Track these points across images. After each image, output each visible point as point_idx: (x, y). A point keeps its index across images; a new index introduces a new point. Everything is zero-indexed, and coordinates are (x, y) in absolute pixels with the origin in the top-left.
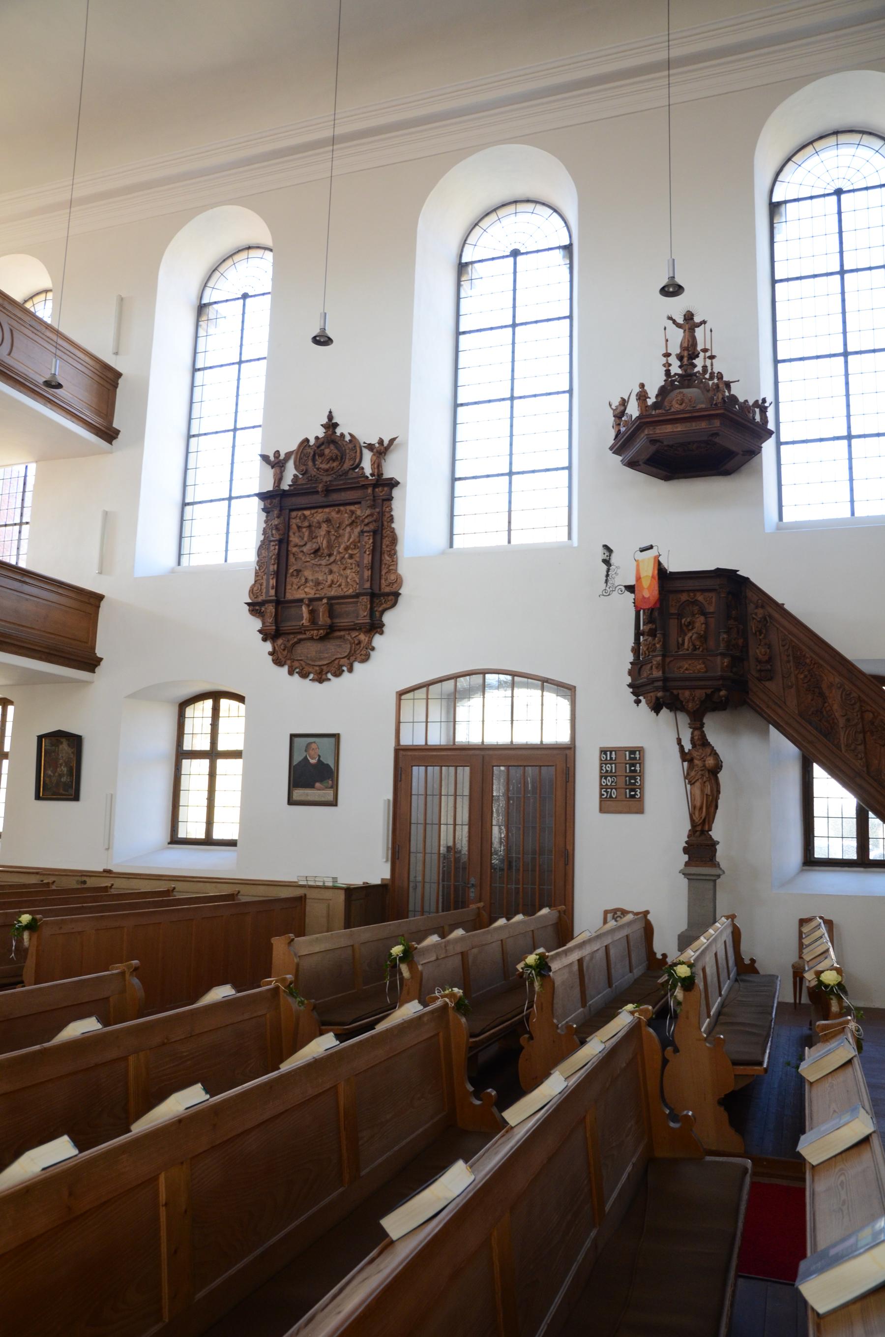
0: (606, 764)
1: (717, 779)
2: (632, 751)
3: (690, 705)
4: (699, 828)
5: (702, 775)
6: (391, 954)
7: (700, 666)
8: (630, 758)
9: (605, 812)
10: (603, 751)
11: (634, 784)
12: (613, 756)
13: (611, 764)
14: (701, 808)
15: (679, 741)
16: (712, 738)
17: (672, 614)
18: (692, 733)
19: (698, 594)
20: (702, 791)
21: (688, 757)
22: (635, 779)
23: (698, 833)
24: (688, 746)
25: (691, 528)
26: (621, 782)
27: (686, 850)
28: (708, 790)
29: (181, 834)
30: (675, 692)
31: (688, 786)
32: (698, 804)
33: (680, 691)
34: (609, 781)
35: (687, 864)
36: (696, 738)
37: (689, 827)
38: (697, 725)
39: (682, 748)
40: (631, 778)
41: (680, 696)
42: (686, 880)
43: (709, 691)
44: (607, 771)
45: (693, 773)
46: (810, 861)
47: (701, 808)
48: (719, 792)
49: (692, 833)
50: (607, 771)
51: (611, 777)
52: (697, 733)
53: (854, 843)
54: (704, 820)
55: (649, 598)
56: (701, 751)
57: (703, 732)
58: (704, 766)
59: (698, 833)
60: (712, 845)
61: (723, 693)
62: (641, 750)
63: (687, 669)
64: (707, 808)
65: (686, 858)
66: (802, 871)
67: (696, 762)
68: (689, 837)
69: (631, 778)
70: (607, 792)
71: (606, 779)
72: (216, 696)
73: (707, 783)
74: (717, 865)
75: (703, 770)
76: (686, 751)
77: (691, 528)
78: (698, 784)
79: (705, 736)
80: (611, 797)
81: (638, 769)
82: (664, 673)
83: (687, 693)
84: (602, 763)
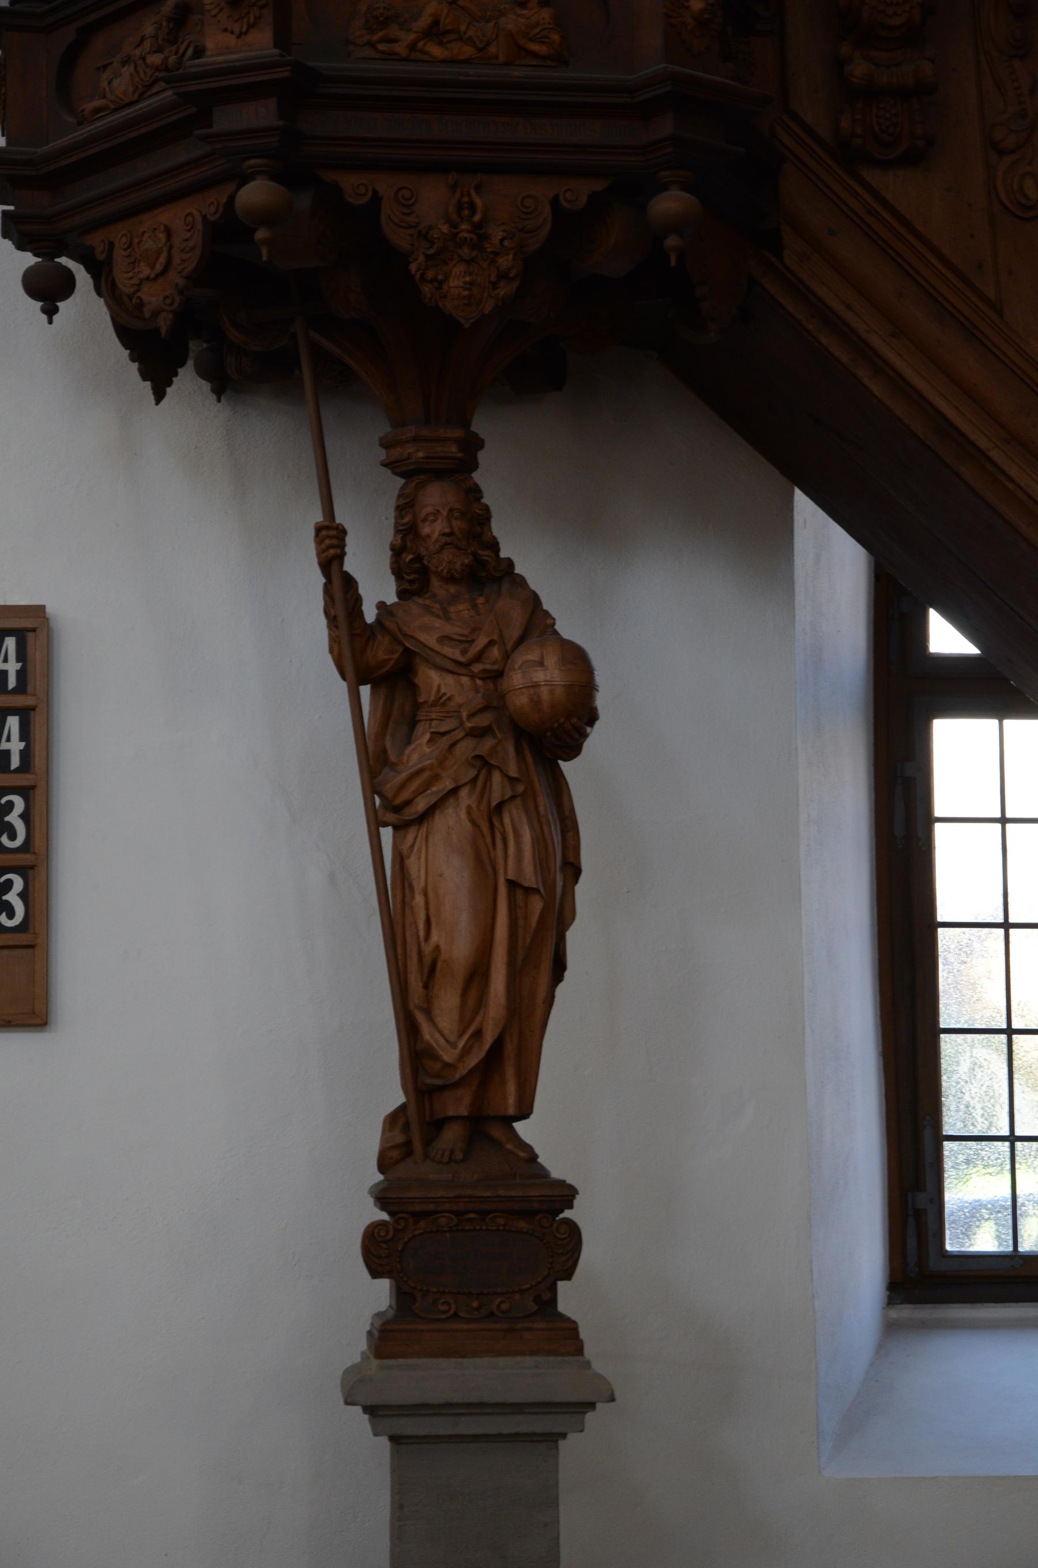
1: (559, 788)
3: (457, 280)
4: (457, 1104)
5: (483, 763)
6: (370, 625)
14: (478, 973)
15: (331, 543)
16: (527, 551)
18: (405, 506)
20: (484, 868)
21: (382, 652)
23: (451, 1136)
24: (377, 588)
27: (379, 1252)
28: (520, 857)
30: (354, 186)
31: (387, 834)
32: (457, 943)
33: (385, 185)
35: (388, 1339)
36: (434, 530)
37: (393, 1095)
38: (436, 467)
39: (341, 593)
42: (384, 1443)
43: (577, 193)
45: (420, 752)
46: (927, 1275)
47: (478, 973)
48: (573, 870)
49: (408, 1138)
52: (436, 497)
54: (498, 1044)
56: (462, 608)
57: (475, 493)
58: (496, 703)
59: (451, 1136)
60: (540, 1225)
61: (670, 203)
63: (434, 32)
64: (514, 974)
65: (379, 1294)
66: (891, 1329)
67: (432, 680)
68: (383, 1165)
72: (439, 1163)
73: (514, 818)
74: (566, 1338)
75: (469, 746)
76: (370, 614)
78: (453, 822)
79: (484, 517)
82: (282, 39)
83: (432, 199)
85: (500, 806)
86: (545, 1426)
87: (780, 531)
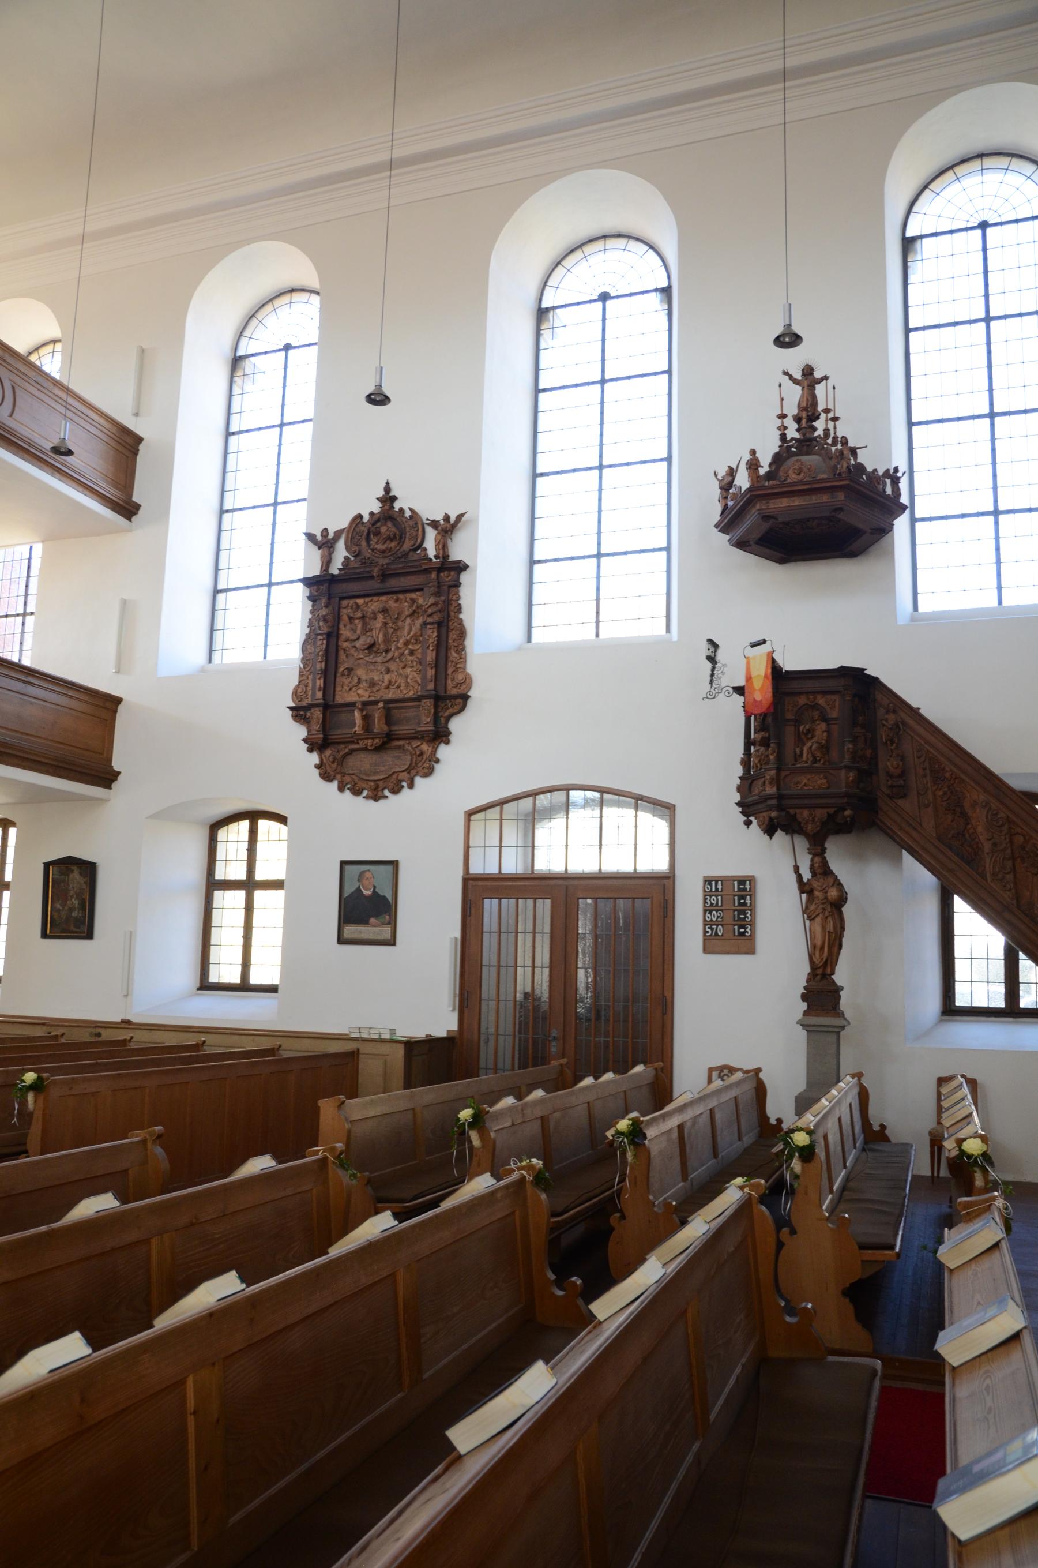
0: (711, 896)
1: (841, 914)
2: (742, 881)
3: (810, 827)
4: (820, 971)
5: (824, 909)
7: (821, 781)
8: (739, 889)
9: (709, 953)
10: (708, 881)
11: (744, 919)
12: (720, 887)
13: (716, 896)
14: (822, 948)
15: (796, 869)
17: (788, 720)
18: (812, 860)
19: (819, 697)
20: (824, 928)
21: (807, 888)
22: (745, 914)
23: (819, 977)
24: (807, 875)
25: (811, 620)
26: (728, 917)
27: (804, 997)
28: (830, 926)
29: (213, 979)
30: (792, 811)
31: (808, 922)
32: (819, 943)
33: (798, 811)
34: (714, 916)
35: (806, 1013)
36: (816, 865)
37: (808, 970)
39: (799, 877)
40: (740, 912)
41: (798, 816)
42: (805, 1032)
43: (831, 811)
44: (712, 904)
45: (813, 907)
46: (950, 1010)
47: (822, 948)
48: (843, 929)
49: (812, 976)
50: (712, 904)
51: (717, 911)
52: (817, 859)
53: (1001, 989)
54: (826, 961)
55: (761, 701)
56: (822, 880)
57: (825, 858)
58: (826, 898)
59: (819, 977)
60: (835, 991)
61: (848, 813)
62: (752, 880)
63: (805, 785)
64: (830, 948)
65: (804, 1006)
66: (941, 1021)
67: (816, 893)
68: (808, 981)
69: (740, 912)
70: (712, 929)
71: (710, 913)
73: (830, 919)
74: (841, 1015)
75: (825, 904)
76: (805, 880)
77: (811, 620)
78: (818, 920)
79: (827, 863)
80: (716, 934)
81: (748, 901)
82: (778, 789)
83: (806, 813)
84: (707, 895)
85: (1018, 898)
86: (837, 1032)
87: (900, 858)
